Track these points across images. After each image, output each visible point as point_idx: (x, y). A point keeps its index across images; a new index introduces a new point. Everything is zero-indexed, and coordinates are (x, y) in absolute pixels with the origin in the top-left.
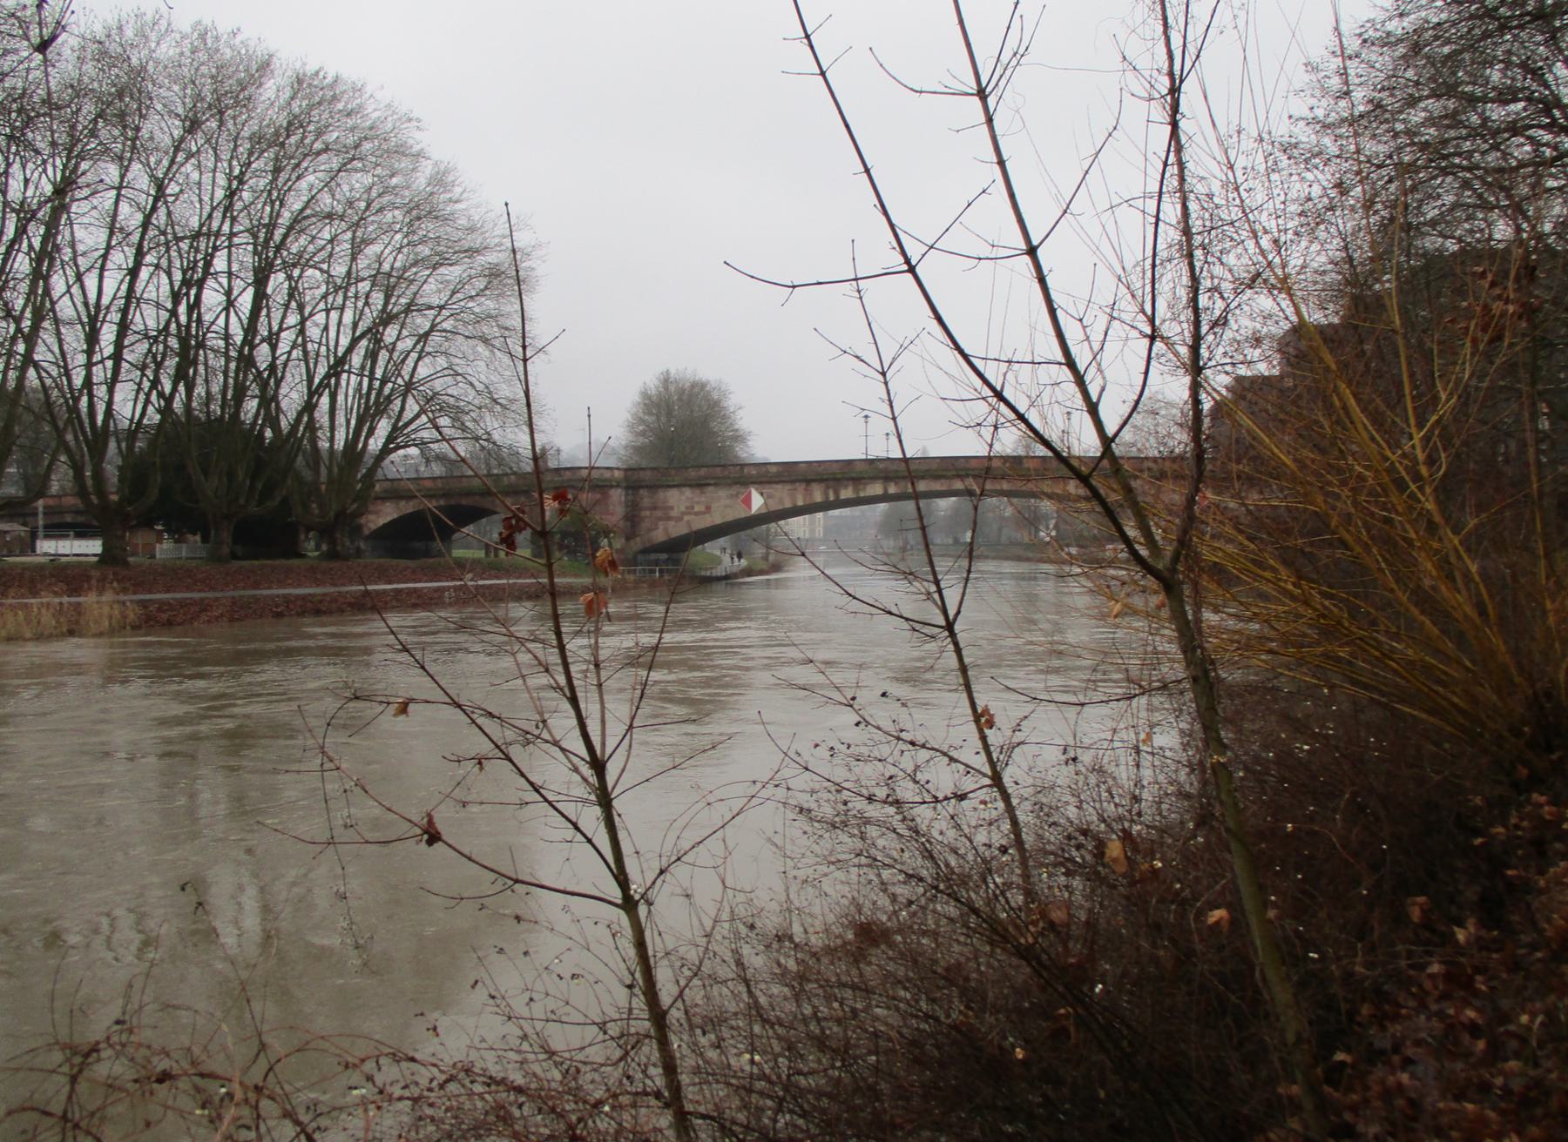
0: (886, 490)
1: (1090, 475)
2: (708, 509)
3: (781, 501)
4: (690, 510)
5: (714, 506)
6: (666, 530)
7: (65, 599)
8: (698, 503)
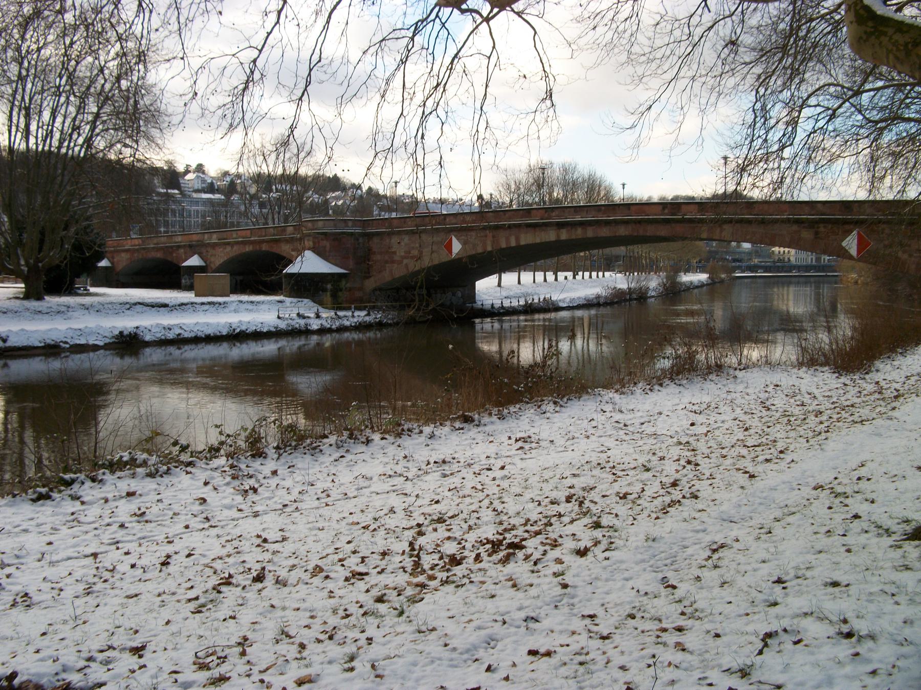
0: (558, 236)
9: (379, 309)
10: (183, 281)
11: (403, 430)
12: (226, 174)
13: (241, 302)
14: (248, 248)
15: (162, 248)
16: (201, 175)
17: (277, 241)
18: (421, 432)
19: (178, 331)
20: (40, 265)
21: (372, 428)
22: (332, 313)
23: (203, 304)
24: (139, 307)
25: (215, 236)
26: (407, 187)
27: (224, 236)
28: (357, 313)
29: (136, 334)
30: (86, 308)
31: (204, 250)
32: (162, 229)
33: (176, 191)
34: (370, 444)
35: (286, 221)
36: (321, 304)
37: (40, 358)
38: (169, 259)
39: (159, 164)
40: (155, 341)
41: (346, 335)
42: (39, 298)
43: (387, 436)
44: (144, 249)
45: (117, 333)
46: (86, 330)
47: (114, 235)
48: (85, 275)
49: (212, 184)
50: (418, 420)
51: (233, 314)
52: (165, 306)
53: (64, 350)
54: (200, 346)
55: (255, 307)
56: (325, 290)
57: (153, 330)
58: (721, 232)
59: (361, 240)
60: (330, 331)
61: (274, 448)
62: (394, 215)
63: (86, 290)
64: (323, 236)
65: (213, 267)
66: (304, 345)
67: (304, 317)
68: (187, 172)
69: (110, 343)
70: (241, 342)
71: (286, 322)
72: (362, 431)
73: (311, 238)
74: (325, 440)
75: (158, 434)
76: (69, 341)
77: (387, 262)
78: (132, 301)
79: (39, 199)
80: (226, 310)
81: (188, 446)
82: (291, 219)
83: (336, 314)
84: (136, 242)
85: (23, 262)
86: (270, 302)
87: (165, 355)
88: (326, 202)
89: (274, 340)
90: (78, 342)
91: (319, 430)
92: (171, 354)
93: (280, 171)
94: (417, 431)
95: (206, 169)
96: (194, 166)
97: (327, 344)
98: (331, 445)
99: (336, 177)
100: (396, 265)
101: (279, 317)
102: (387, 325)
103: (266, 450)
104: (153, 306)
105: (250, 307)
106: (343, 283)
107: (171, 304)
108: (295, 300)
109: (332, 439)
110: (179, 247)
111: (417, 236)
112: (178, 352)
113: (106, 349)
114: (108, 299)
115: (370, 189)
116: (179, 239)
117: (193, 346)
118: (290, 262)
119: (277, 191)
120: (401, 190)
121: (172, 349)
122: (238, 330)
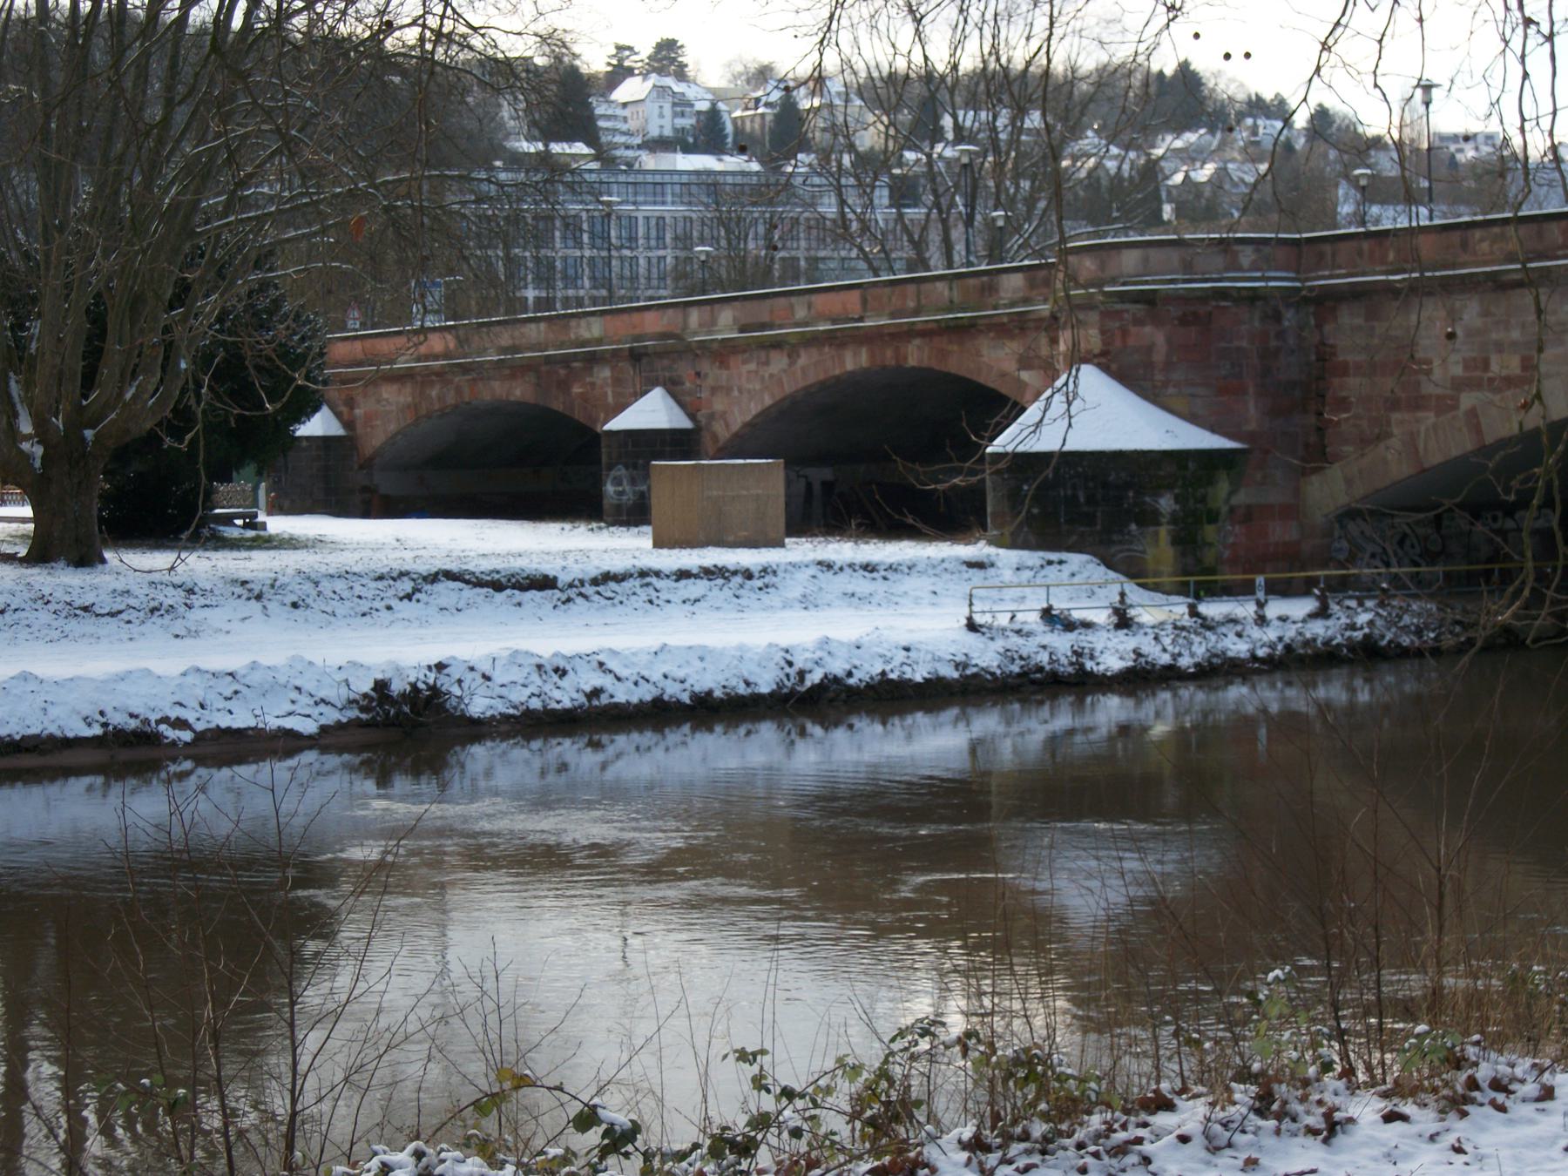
4: (1476, 376)
8: (1500, 347)
9: (1364, 590)
10: (610, 488)
11: (1473, 1084)
12: (763, 74)
13: (827, 566)
14: (854, 360)
15: (529, 367)
16: (669, 81)
17: (962, 331)
18: (1548, 1094)
19: (592, 680)
20: (89, 434)
21: (1348, 1073)
22: (1178, 609)
23: (683, 574)
24: (446, 592)
25: (726, 316)
26: (1483, 109)
27: (762, 312)
28: (1275, 608)
29: (435, 690)
30: (253, 593)
31: (684, 370)
32: (531, 294)
33: (580, 148)
34: (1340, 1140)
35: (996, 250)
36: (1135, 571)
37: (86, 780)
38: (557, 405)
39: (515, 48)
40: (506, 718)
41: (1236, 693)
42: (86, 558)
43: (1408, 1108)
44: (466, 369)
45: (366, 686)
46: (254, 679)
47: (354, 319)
48: (250, 469)
49: (713, 116)
50: (1533, 1045)
51: (797, 614)
52: (544, 583)
53: (175, 751)
54: (673, 737)
55: (880, 586)
56: (1149, 518)
57: (499, 677)
59: (1289, 318)
60: (1170, 676)
61: (964, 1146)
62: (1423, 216)
63: (252, 525)
64: (1138, 309)
65: (723, 432)
66: (1071, 732)
67: (1069, 626)
68: (619, 73)
69: (339, 726)
70: (829, 723)
71: (999, 644)
72: (1306, 1083)
73: (1094, 317)
74: (1162, 1119)
75: (522, 1082)
76: (190, 716)
77: (1394, 404)
78: (424, 568)
79: (86, 188)
80: (772, 598)
81: (635, 1130)
82: (1014, 242)
83: (1194, 613)
84: (436, 343)
85: (26, 427)
86: (937, 568)
87: (543, 773)
88: (1151, 172)
89: (953, 712)
90: (225, 721)
91: (1136, 1072)
92: (563, 767)
93: (969, 62)
94: (1531, 1089)
95: (689, 57)
96: (645, 49)
97: (1160, 729)
98: (1184, 1139)
99: (1186, 75)
100: (1429, 417)
101: (972, 626)
102: (1399, 654)
103: (931, 1152)
104: (498, 586)
105: (862, 584)
106: (1221, 491)
107: (564, 579)
108: (1032, 558)
109: (1191, 1114)
110: (592, 359)
111: (1525, 298)
112: (590, 759)
113: (325, 750)
114: (336, 561)
115: (1322, 116)
116: (594, 329)
117: (648, 738)
118: (1003, 408)
119: (961, 135)
120: (1448, 118)
121: (567, 748)
122: (815, 677)
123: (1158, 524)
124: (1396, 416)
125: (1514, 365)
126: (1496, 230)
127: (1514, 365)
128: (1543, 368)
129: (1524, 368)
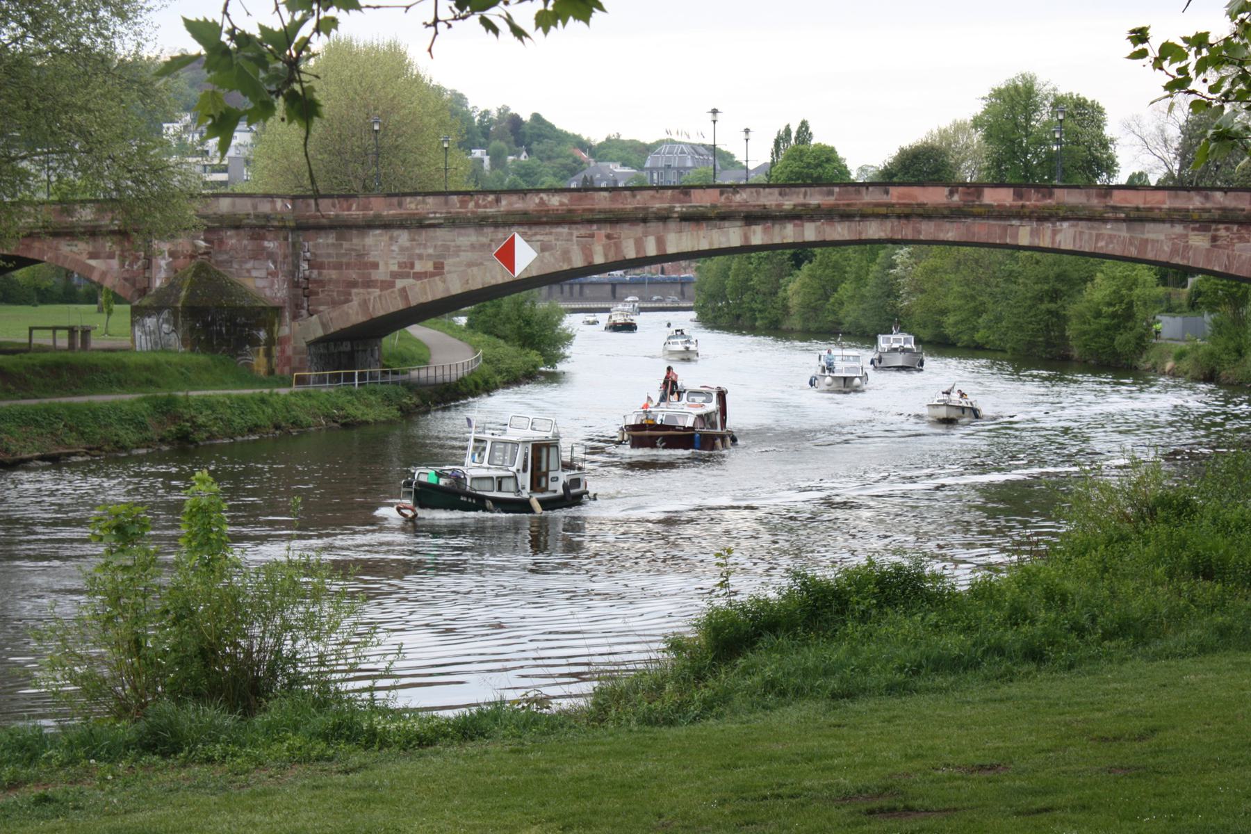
0: (746, 237)
1: (54, 334)
2: (439, 268)
3: (566, 255)
4: (406, 269)
5: (449, 263)
6: (364, 304)
7: (357, 382)
8: (420, 257)
58: (1055, 233)
77: (354, 284)
100: (377, 292)
123: (260, 345)
124: (354, 291)
125: (429, 266)
126: (420, 198)
127: (429, 266)
128: (446, 268)
129: (435, 268)
